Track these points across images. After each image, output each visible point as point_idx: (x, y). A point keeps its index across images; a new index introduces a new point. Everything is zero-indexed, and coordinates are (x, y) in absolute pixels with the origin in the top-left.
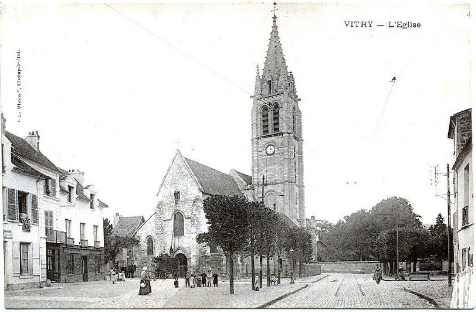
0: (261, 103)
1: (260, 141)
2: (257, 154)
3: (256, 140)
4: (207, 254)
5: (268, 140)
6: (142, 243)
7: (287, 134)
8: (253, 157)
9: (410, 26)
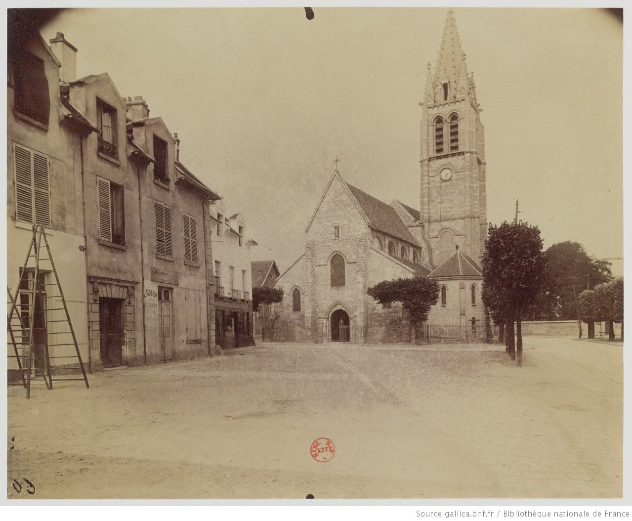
1: (432, 163)
2: (428, 179)
3: (427, 162)
4: (378, 310)
5: (443, 161)
6: (284, 296)
7: (469, 154)
8: (422, 184)
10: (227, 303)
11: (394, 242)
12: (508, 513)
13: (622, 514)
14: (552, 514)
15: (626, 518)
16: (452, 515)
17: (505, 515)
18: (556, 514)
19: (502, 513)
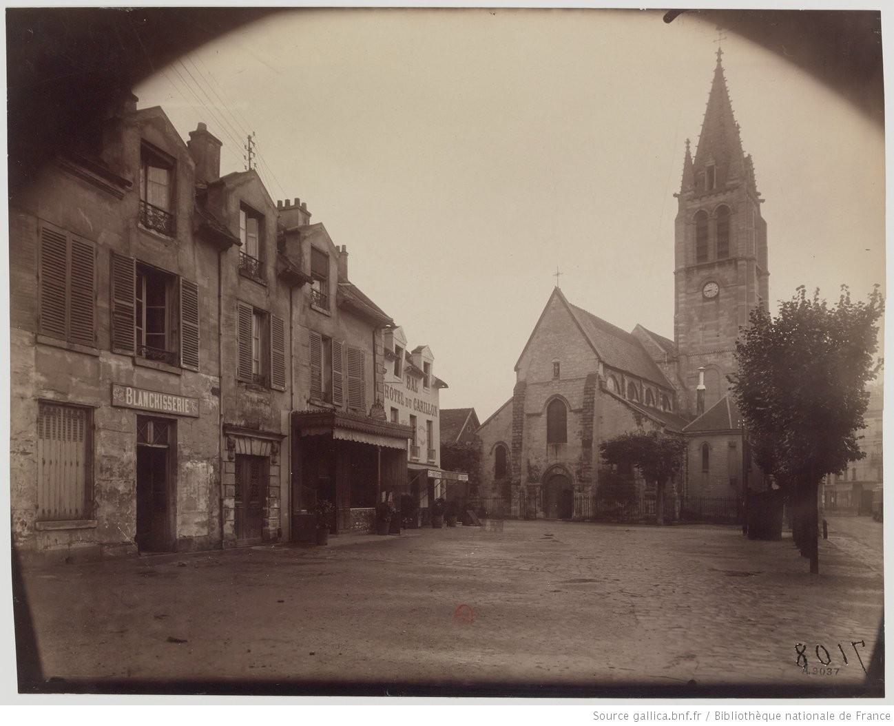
0: (697, 205)
5: (704, 273)
9: (63, 300)
11: (636, 382)
12: (720, 715)
13: (879, 716)
14: (783, 716)
15: (886, 722)
17: (718, 717)
18: (788, 716)
19: (713, 716)
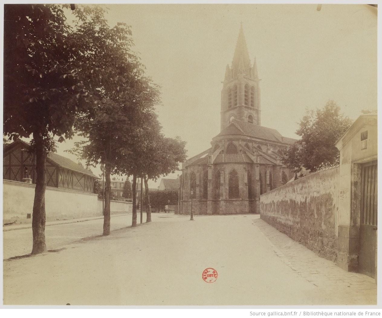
10: (190, 183)
14: (333, 314)
16: (339, 315)
18: (336, 314)
